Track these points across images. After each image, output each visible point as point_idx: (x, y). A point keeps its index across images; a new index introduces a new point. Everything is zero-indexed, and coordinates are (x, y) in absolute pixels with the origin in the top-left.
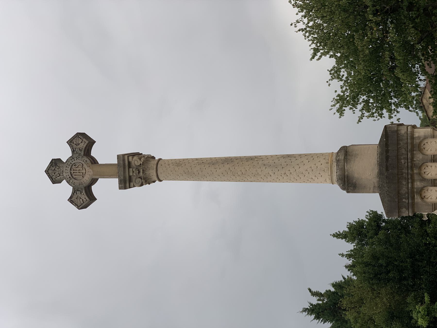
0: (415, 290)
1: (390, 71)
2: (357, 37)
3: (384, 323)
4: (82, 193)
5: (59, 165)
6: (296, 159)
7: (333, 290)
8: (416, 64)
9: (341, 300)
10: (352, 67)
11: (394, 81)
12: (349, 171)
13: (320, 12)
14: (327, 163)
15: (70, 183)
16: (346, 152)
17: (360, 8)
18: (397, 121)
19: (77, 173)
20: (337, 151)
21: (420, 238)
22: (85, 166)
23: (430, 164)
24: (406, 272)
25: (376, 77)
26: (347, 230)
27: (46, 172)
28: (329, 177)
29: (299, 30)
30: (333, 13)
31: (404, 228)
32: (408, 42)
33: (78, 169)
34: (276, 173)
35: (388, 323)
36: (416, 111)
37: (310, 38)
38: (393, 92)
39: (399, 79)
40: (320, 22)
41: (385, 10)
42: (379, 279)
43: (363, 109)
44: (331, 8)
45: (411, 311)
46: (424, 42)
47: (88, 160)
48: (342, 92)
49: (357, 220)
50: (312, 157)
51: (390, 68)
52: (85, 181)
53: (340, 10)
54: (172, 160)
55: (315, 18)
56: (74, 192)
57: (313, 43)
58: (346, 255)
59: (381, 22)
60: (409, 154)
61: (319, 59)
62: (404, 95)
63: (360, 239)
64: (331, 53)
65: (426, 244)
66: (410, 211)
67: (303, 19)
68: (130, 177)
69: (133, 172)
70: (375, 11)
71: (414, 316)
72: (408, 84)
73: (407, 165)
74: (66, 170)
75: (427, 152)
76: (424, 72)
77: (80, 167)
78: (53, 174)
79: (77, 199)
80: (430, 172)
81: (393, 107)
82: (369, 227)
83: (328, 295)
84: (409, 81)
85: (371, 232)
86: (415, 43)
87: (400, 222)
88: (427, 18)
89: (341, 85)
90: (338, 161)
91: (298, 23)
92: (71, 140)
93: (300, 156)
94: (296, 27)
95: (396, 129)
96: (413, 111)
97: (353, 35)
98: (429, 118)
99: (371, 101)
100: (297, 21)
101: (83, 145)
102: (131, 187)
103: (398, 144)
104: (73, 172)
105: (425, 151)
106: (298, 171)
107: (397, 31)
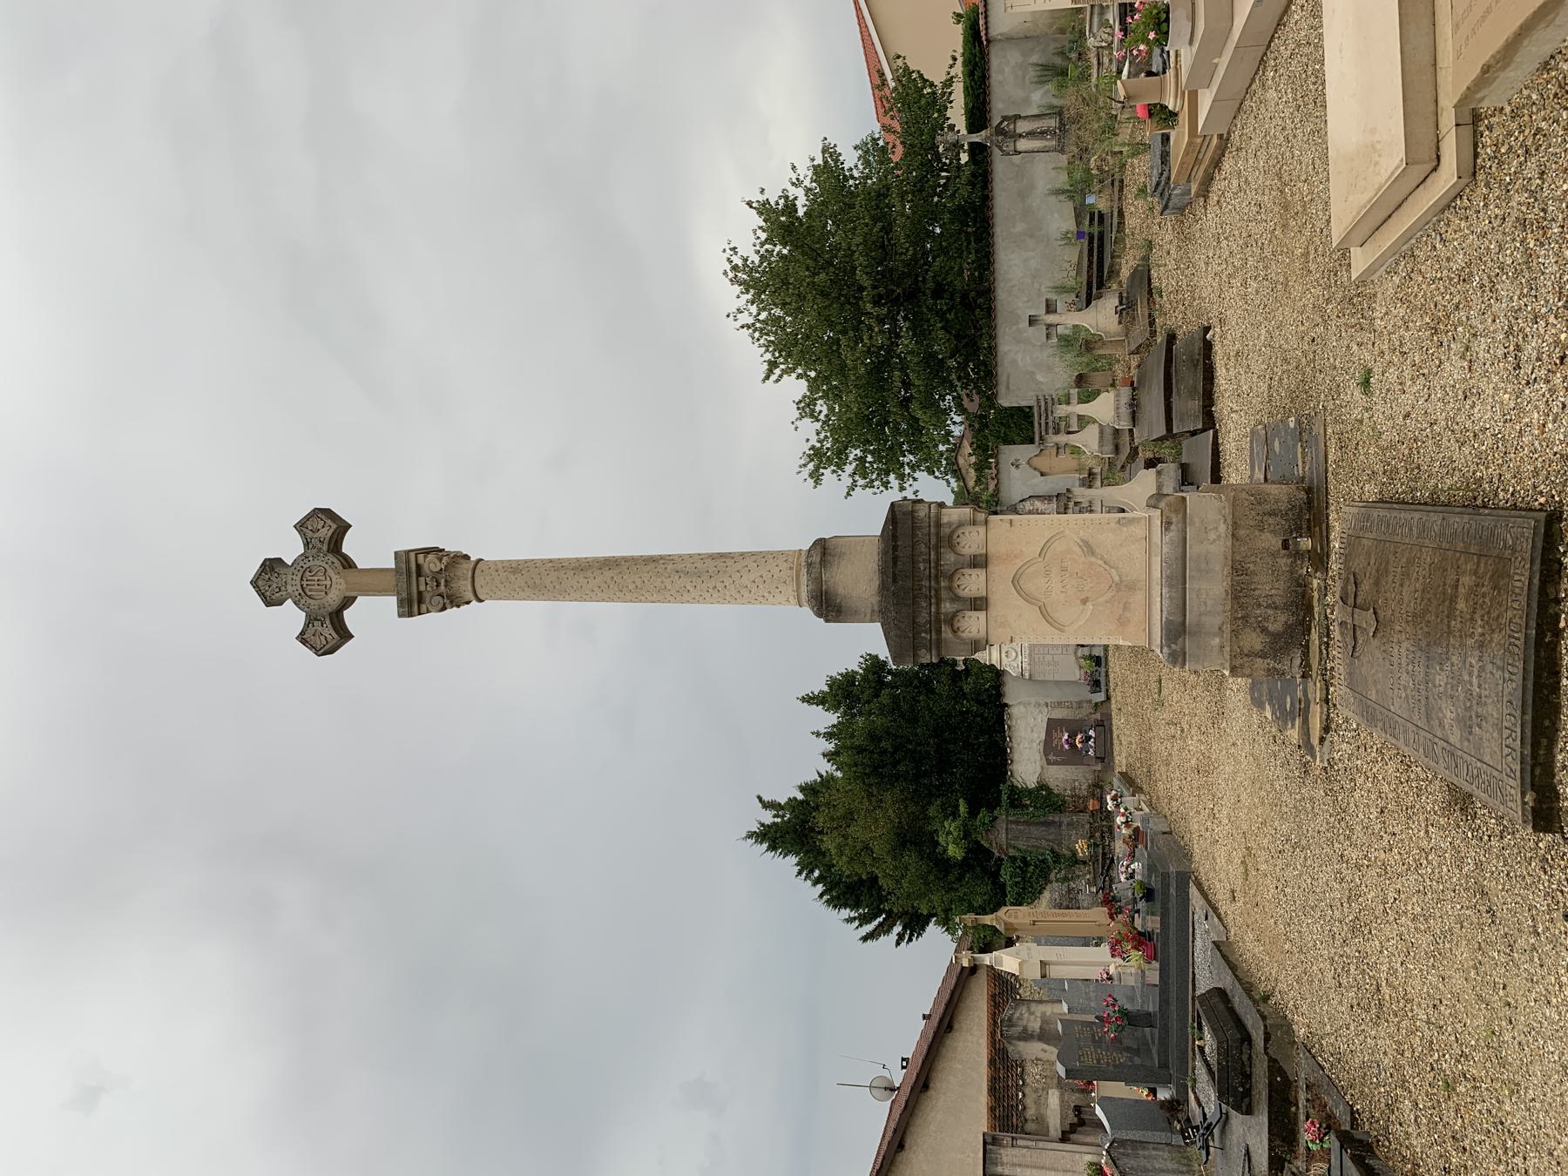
0: (943, 795)
1: (902, 405)
4: (325, 625)
7: (800, 797)
8: (947, 394)
9: (814, 814)
11: (908, 424)
14: (791, 568)
16: (825, 549)
19: (314, 585)
22: (330, 572)
23: (967, 571)
26: (826, 689)
29: (742, 327)
32: (933, 355)
33: (316, 578)
34: (698, 587)
37: (762, 341)
41: (894, 296)
42: (882, 776)
43: (854, 473)
47: (335, 560)
48: (818, 442)
52: (331, 602)
53: (814, 292)
57: (767, 351)
58: (825, 733)
59: (886, 316)
60: (932, 553)
61: (777, 381)
64: (800, 371)
65: (961, 713)
67: (749, 306)
68: (420, 593)
69: (427, 584)
71: (941, 840)
76: (961, 410)
77: (319, 573)
78: (267, 588)
81: (907, 471)
84: (934, 425)
87: (917, 673)
90: (809, 565)
94: (735, 320)
99: (869, 458)
100: (738, 310)
101: (326, 533)
103: (914, 535)
105: (959, 549)
107: (914, 335)
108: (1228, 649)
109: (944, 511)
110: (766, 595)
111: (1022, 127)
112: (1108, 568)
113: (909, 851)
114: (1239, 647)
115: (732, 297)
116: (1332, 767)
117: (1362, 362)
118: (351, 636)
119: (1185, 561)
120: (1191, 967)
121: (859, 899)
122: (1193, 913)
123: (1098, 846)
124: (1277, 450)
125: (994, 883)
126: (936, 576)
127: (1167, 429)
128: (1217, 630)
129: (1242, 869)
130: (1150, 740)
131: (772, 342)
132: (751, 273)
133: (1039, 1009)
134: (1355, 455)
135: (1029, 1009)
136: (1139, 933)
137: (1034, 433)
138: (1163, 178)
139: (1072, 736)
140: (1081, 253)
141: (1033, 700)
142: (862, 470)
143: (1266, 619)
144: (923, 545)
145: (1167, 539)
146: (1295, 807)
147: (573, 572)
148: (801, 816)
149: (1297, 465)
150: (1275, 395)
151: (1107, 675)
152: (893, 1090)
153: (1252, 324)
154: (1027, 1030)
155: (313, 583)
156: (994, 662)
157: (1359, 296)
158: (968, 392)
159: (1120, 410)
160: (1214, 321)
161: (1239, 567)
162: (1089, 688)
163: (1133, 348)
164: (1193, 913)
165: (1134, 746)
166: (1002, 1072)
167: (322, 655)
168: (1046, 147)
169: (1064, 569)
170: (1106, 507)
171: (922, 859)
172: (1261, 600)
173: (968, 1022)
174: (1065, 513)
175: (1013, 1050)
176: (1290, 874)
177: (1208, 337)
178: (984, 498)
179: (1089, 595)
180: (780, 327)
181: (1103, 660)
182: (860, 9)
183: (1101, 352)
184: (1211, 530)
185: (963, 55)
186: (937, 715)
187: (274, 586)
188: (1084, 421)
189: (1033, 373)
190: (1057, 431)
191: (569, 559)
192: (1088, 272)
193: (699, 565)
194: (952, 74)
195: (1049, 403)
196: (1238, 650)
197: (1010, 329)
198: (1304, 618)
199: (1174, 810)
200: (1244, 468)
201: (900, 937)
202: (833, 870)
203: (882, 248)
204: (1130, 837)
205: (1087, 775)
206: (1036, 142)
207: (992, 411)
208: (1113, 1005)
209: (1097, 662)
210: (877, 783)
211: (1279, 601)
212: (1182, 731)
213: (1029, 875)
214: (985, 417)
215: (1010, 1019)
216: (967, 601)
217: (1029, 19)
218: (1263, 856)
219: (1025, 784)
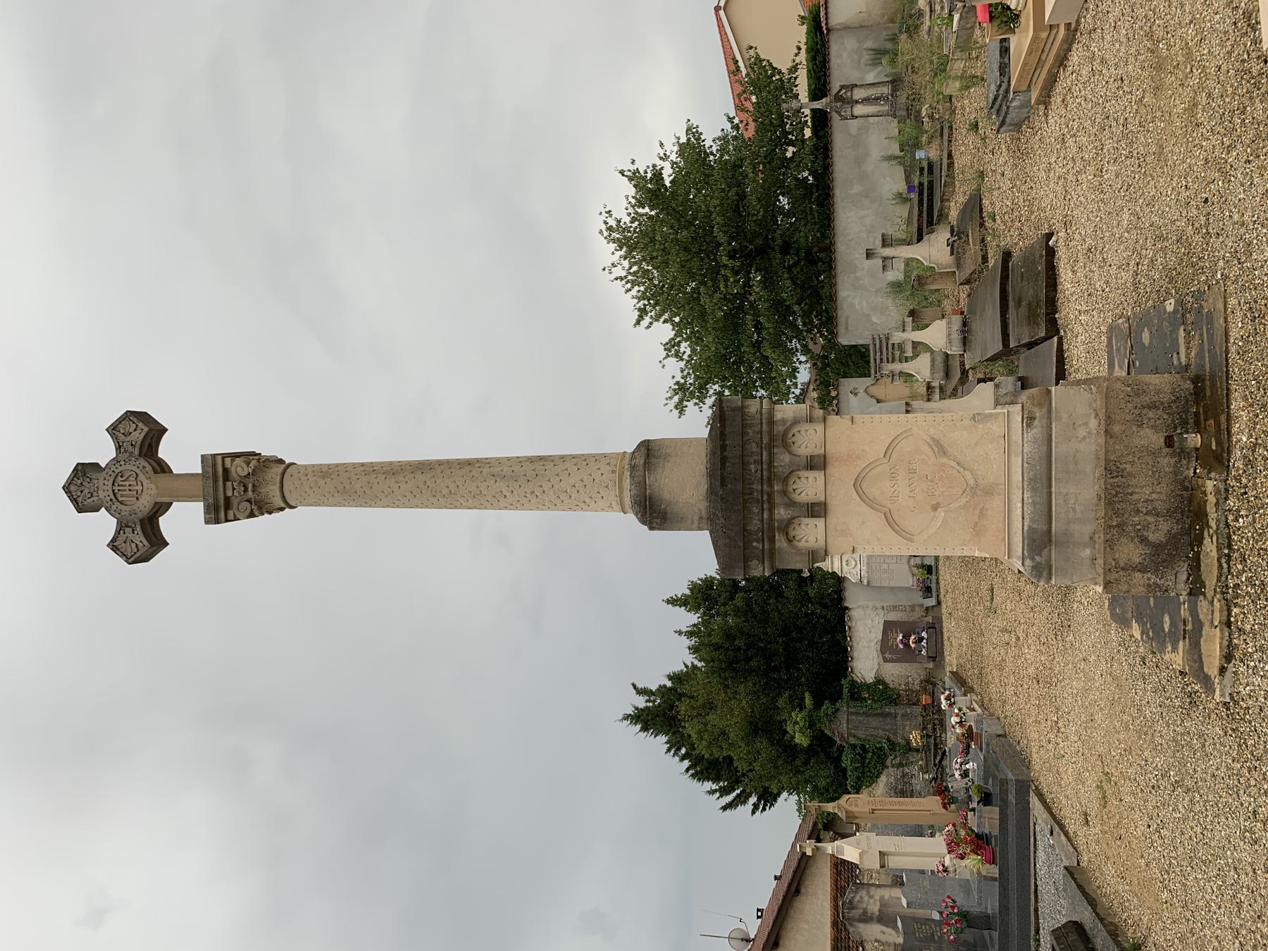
0: (791, 688)
4: (136, 532)
5: (91, 475)
6: (555, 465)
7: (669, 684)
9: (677, 703)
14: (613, 472)
15: (112, 511)
16: (648, 450)
19: (125, 490)
22: (142, 477)
23: (803, 474)
26: (688, 592)
27: (64, 489)
29: (616, 279)
32: (781, 302)
33: (127, 483)
34: (515, 492)
41: (747, 252)
44: (664, 244)
47: (146, 465)
48: (682, 378)
50: (585, 460)
52: (142, 508)
54: (313, 466)
56: (121, 528)
60: (765, 453)
61: (648, 327)
65: (807, 614)
66: (766, 566)
67: (622, 261)
68: (227, 499)
69: (234, 489)
71: (789, 728)
73: (759, 475)
74: (104, 484)
76: (806, 350)
77: (131, 478)
78: (79, 494)
79: (125, 542)
80: (802, 490)
90: (633, 468)
92: (115, 425)
93: (562, 458)
94: (610, 273)
99: (727, 393)
100: (612, 264)
101: (137, 436)
102: (229, 519)
103: (744, 434)
104: (118, 490)
105: (794, 449)
108: (1100, 561)
110: (587, 500)
111: (859, 94)
112: (961, 470)
113: (761, 737)
115: (608, 253)
118: (168, 544)
119: (1051, 461)
120: (1032, 878)
121: (720, 774)
122: (1035, 824)
123: (930, 736)
125: (835, 767)
126: (769, 479)
127: (1003, 344)
130: (982, 644)
132: (624, 232)
133: (878, 893)
135: (868, 892)
136: (977, 835)
138: (1001, 92)
139: (907, 637)
140: (910, 213)
141: (871, 604)
143: (1146, 527)
144: (754, 444)
145: (1029, 436)
148: (669, 702)
149: (1178, 353)
151: (938, 583)
152: (748, 941)
154: (867, 913)
155: (124, 488)
156: (835, 570)
159: (952, 337)
160: (1057, 227)
162: (921, 593)
164: (1035, 824)
165: (965, 649)
166: (844, 933)
167: (133, 563)
168: (879, 111)
171: (772, 745)
172: (1140, 505)
173: (814, 887)
175: (854, 932)
177: (1050, 243)
179: (941, 500)
182: (720, 19)
184: (1080, 425)
185: (806, 44)
186: (785, 616)
187: (86, 491)
189: (869, 315)
193: (517, 468)
194: (797, 61)
197: (848, 277)
199: (1009, 714)
201: (756, 807)
203: (737, 208)
204: (963, 735)
205: (919, 671)
206: (870, 107)
208: (953, 907)
209: (928, 570)
210: (731, 677)
211: (1160, 506)
212: (1018, 639)
213: (867, 761)
214: (827, 357)
215: (851, 902)
217: (864, 9)
219: (864, 679)
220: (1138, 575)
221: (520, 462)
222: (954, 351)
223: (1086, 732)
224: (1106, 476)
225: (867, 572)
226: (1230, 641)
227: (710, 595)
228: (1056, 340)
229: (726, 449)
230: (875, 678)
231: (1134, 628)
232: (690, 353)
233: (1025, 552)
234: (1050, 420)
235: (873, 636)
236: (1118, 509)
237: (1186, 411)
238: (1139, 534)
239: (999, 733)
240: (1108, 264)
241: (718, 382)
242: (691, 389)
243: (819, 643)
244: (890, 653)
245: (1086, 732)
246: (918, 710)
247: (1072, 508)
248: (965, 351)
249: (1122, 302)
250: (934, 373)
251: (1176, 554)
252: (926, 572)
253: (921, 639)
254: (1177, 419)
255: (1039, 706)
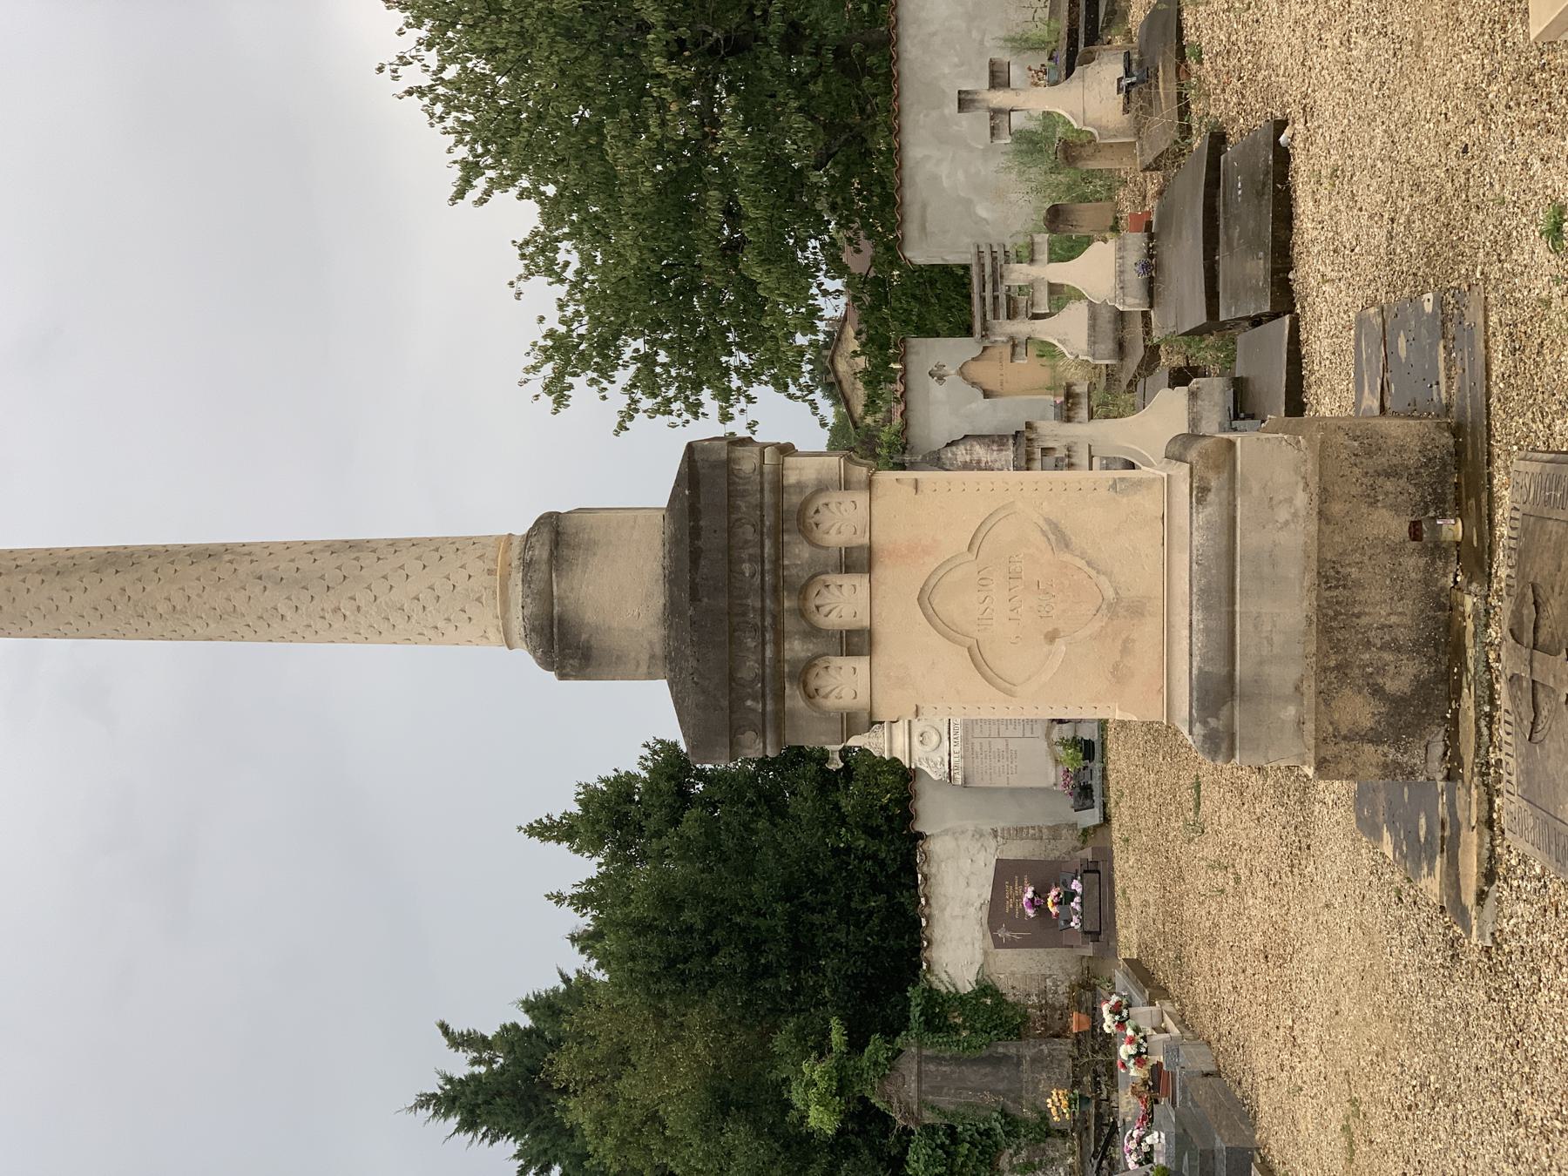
0: (801, 1010)
1: (724, 256)
2: (613, 133)
3: (695, 1131)
6: (379, 559)
7: (525, 1021)
8: (811, 237)
9: (550, 1055)
10: (597, 238)
11: (737, 293)
12: (566, 602)
13: (483, 31)
16: (558, 533)
17: (623, 29)
18: (748, 431)
20: (525, 532)
21: (818, 831)
23: (834, 579)
24: (771, 949)
25: (676, 276)
26: (576, 809)
28: (495, 621)
29: (410, 93)
30: (529, 40)
31: (767, 802)
32: (782, 161)
34: (303, 609)
35: (708, 1127)
36: (810, 397)
37: (450, 122)
38: (735, 331)
39: (753, 285)
40: (484, 69)
41: (707, 45)
42: (683, 978)
43: (633, 386)
44: (521, 20)
45: (786, 1081)
46: (836, 164)
48: (562, 322)
49: (612, 774)
51: (724, 249)
53: (552, 30)
55: (466, 51)
57: (460, 141)
58: (572, 897)
59: (694, 82)
60: (768, 543)
61: (481, 201)
62: (769, 343)
63: (618, 840)
64: (525, 183)
65: (836, 851)
66: (768, 741)
70: (676, 45)
71: (796, 1097)
72: (785, 303)
75: (826, 536)
76: (838, 268)
80: (832, 606)
81: (736, 382)
82: (651, 796)
83: (507, 1042)
84: (786, 296)
85: (658, 816)
86: (808, 166)
87: (754, 776)
88: (848, 81)
89: (559, 299)
90: (528, 565)
91: (405, 64)
94: (395, 78)
95: (726, 456)
96: (799, 397)
97: (601, 124)
98: (855, 423)
99: (663, 357)
100: (400, 58)
103: (731, 508)
105: (818, 535)
106: (386, 603)
107: (748, 122)
108: (1310, 726)
109: (790, 461)
112: (1093, 573)
113: (735, 1121)
114: (1331, 723)
116: (1499, 947)
117: (1549, 191)
119: (1234, 560)
124: (1403, 353)
128: (1293, 689)
129: (1343, 1141)
130: (1181, 897)
131: (469, 124)
134: (1537, 364)
137: (971, 314)
139: (1041, 893)
141: (970, 825)
142: (647, 379)
143: (1381, 670)
146: (1436, 1023)
147: (39, 578)
149: (1438, 383)
150: (1398, 251)
151: (1104, 777)
153: (1360, 118)
157: (1543, 70)
158: (850, 234)
160: (1294, 110)
161: (1332, 573)
162: (1072, 800)
163: (1149, 159)
165: (1152, 910)
169: (1014, 576)
170: (1102, 458)
174: (1028, 469)
176: (1427, 1148)
177: (1282, 139)
178: (884, 437)
180: (485, 96)
181: (1097, 747)
183: (1093, 165)
188: (1060, 295)
190: (1012, 315)
191: (31, 552)
192: (1070, 13)
195: (999, 260)
196: (1331, 729)
197: (926, 116)
198: (1450, 668)
199: (1224, 1030)
200: (1345, 386)
202: (587, 1164)
204: (1145, 1083)
207: (896, 273)
211: (1403, 635)
212: (1237, 880)
213: (960, 1160)
216: (833, 635)
218: (1379, 1115)
219: (954, 986)
220: (1369, 748)
221: (311, 553)
222: (1129, 306)
223: (1330, 1035)
224: (1319, 585)
225: (964, 757)
226: (1492, 850)
227: (627, 814)
228: (1287, 322)
229: (700, 534)
230: (977, 981)
231: (1385, 841)
232: (579, 266)
233: (1194, 711)
234: (1234, 495)
235: (974, 892)
236: (1338, 640)
237: (1443, 481)
238: (1371, 681)
239: (1206, 1069)
240: (1359, 206)
241: (644, 334)
242: (581, 348)
243: (861, 912)
244: (1008, 929)
245: (1330, 1035)
246: (1065, 1046)
247: (1267, 637)
248: (1151, 306)
249: (1375, 277)
250: (1095, 343)
251: (1426, 714)
252: (1081, 755)
253: (1071, 895)
254: (1430, 495)
255: (1267, 1004)
